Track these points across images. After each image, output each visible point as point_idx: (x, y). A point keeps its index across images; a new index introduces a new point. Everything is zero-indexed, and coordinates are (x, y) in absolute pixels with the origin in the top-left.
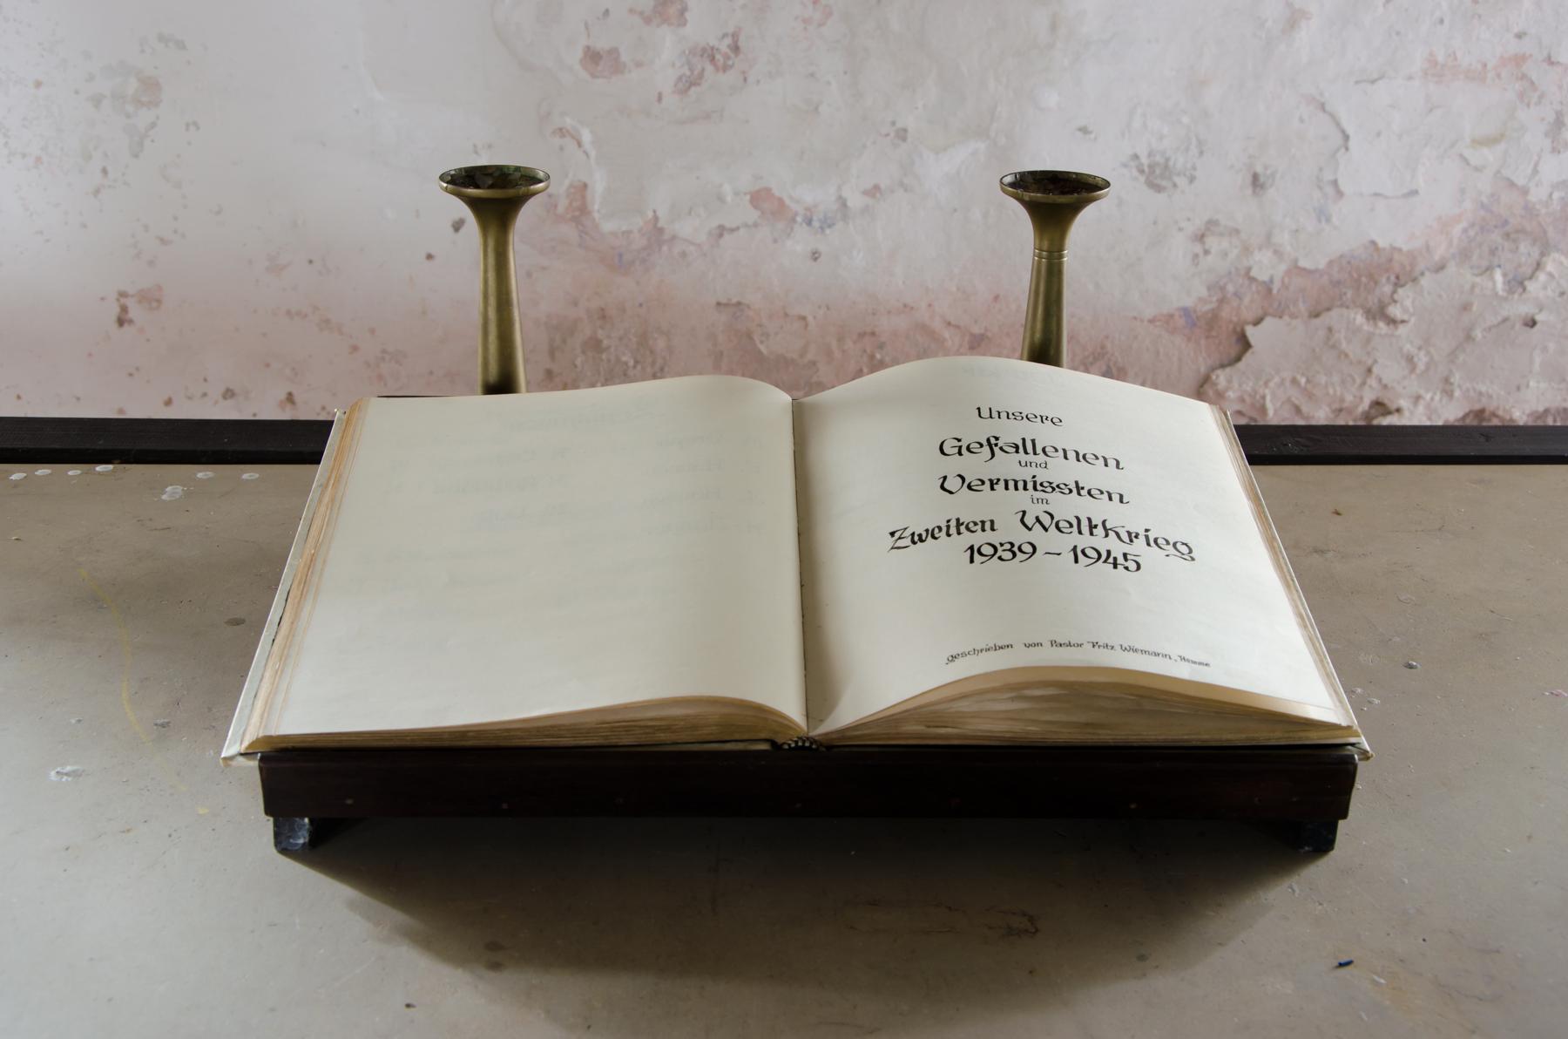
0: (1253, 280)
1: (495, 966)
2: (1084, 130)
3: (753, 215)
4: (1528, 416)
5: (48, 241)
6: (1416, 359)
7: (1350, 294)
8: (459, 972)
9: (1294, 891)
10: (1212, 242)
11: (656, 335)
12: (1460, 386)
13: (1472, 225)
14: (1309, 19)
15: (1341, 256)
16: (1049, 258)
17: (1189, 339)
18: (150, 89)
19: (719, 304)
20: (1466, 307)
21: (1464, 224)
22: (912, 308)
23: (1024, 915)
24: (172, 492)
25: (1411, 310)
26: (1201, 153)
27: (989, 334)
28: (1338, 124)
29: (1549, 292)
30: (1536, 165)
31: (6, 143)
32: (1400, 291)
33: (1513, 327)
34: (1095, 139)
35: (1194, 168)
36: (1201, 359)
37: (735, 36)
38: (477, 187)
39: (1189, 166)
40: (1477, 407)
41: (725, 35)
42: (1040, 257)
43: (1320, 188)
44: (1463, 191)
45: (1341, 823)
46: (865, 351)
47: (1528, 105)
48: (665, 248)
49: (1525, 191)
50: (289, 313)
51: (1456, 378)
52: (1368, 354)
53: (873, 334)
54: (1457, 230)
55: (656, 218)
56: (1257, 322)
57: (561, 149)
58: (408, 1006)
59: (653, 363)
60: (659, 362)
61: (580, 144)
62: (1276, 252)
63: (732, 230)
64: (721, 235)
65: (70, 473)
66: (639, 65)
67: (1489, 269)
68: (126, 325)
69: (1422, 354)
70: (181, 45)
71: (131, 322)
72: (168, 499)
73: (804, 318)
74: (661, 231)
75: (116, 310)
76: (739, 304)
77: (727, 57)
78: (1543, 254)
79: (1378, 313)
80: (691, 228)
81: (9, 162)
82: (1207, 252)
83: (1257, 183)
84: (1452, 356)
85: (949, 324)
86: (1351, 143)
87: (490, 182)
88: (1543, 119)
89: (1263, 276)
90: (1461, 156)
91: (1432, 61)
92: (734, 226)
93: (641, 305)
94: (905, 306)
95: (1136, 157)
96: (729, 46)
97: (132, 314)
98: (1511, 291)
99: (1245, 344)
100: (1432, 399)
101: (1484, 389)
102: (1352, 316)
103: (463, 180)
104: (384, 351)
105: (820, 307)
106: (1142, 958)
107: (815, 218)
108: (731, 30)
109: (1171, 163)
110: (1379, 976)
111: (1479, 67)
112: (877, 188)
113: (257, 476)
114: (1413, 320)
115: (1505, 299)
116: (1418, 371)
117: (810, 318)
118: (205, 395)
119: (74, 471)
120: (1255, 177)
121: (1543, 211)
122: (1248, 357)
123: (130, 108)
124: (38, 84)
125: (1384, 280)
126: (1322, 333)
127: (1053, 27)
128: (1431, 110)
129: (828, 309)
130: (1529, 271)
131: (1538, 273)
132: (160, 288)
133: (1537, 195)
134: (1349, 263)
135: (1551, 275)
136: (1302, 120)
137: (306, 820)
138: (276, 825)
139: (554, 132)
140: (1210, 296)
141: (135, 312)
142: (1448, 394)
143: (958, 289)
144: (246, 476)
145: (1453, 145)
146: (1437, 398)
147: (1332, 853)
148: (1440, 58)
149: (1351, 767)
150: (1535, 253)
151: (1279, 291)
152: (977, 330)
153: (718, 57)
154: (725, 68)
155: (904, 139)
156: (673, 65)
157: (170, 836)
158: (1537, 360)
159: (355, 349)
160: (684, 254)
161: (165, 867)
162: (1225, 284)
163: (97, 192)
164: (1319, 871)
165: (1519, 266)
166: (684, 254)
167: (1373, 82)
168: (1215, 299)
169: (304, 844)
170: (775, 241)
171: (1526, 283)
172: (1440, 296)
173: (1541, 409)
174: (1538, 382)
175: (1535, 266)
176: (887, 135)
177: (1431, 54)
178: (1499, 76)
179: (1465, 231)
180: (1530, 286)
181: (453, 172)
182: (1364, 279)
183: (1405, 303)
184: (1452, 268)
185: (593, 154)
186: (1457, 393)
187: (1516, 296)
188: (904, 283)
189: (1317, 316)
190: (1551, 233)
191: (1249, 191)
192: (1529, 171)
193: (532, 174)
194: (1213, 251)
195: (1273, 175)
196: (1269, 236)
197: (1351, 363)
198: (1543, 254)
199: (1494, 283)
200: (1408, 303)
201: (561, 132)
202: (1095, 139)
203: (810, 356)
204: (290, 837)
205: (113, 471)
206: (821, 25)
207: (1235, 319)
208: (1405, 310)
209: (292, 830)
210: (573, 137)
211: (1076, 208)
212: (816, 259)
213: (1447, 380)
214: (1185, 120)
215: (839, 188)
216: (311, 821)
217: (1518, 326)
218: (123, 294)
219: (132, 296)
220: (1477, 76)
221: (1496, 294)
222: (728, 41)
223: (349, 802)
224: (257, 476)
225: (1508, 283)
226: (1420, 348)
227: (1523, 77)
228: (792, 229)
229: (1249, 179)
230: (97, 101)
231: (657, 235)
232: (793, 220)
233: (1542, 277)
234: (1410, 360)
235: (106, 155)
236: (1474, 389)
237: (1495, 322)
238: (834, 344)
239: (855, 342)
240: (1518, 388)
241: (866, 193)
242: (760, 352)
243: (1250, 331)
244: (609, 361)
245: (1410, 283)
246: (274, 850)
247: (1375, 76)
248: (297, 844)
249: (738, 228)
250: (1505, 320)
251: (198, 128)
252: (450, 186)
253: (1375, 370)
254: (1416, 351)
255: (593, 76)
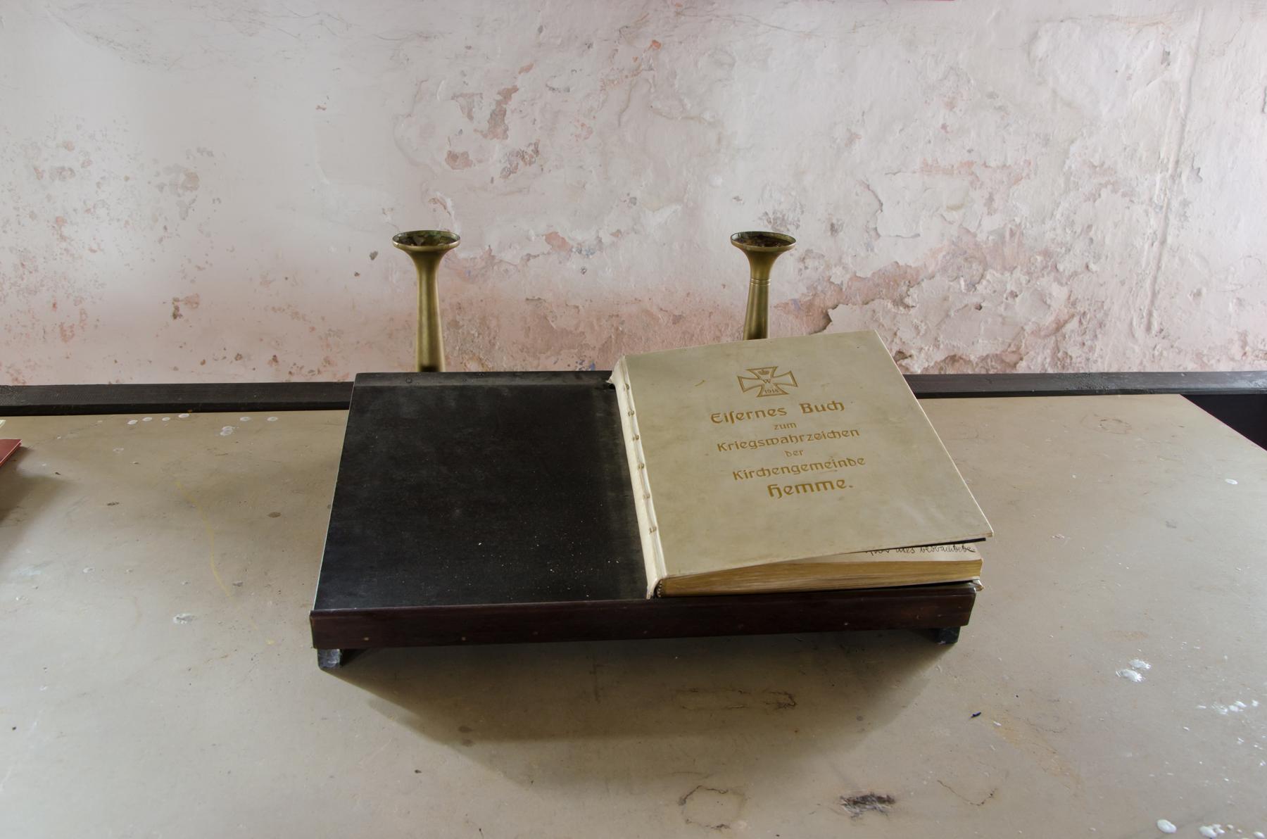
0: (832, 283)
1: (467, 743)
2: (737, 199)
3: (547, 248)
4: (978, 358)
5: (132, 269)
6: (920, 328)
7: (884, 291)
8: (446, 747)
9: (939, 670)
10: (809, 262)
11: (491, 318)
12: (943, 343)
13: (948, 253)
14: (860, 138)
15: (880, 270)
16: (760, 284)
17: (797, 317)
18: (192, 180)
19: (527, 299)
20: (946, 299)
21: (944, 253)
22: (640, 301)
23: (786, 694)
24: (226, 430)
25: (917, 300)
26: (803, 212)
27: (684, 315)
28: (877, 197)
29: (988, 291)
30: (980, 222)
31: (108, 213)
32: (911, 289)
33: (970, 309)
34: (744, 203)
35: (799, 221)
36: (803, 329)
37: (536, 145)
38: (415, 244)
39: (796, 219)
40: (952, 354)
41: (530, 144)
42: (755, 283)
43: (867, 232)
44: (943, 235)
45: (963, 628)
46: (613, 326)
47: (975, 189)
48: (495, 267)
49: (975, 236)
50: (273, 308)
51: (941, 338)
52: (895, 324)
53: (618, 316)
54: (940, 257)
55: (490, 250)
56: (835, 307)
57: (434, 210)
58: (417, 772)
59: (490, 334)
60: (493, 334)
61: (445, 208)
62: (844, 268)
63: (535, 257)
64: (528, 260)
65: (164, 419)
66: (480, 161)
67: (957, 278)
68: (178, 318)
69: (923, 324)
70: (210, 154)
71: (181, 316)
72: (224, 435)
73: (577, 307)
74: (493, 257)
75: (172, 309)
76: (539, 299)
77: (531, 157)
78: (984, 270)
79: (900, 302)
80: (511, 256)
81: (110, 224)
82: (806, 268)
83: (833, 229)
84: (939, 326)
85: (661, 309)
86: (884, 207)
87: (422, 240)
88: (983, 197)
89: (837, 282)
90: (942, 215)
91: (925, 163)
92: (536, 254)
93: (482, 301)
94: (636, 299)
95: (766, 214)
96: (532, 150)
97: (181, 311)
98: (969, 290)
99: (828, 320)
100: (929, 349)
101: (955, 344)
102: (885, 304)
103: (408, 240)
104: (330, 330)
105: (586, 300)
106: (860, 719)
107: (583, 249)
108: (533, 141)
109: (786, 218)
110: (997, 721)
111: (950, 167)
112: (619, 231)
113: (276, 419)
114: (918, 306)
115: (966, 294)
116: (921, 334)
117: (581, 307)
118: (225, 358)
119: (166, 418)
120: (832, 225)
121: (984, 246)
122: (829, 327)
123: (180, 191)
124: (127, 179)
125: (902, 283)
126: (870, 313)
127: (719, 141)
128: (925, 190)
129: (591, 301)
130: (978, 279)
131: (982, 280)
132: (198, 296)
133: (981, 237)
134: (884, 274)
135: (988, 281)
136: (857, 194)
137: (338, 650)
138: (319, 653)
139: (430, 201)
140: (808, 293)
141: (183, 310)
142: (937, 347)
143: (666, 290)
144: (270, 419)
145: (937, 210)
146: (931, 349)
147: (957, 644)
148: (930, 162)
149: (972, 595)
150: (981, 271)
151: (846, 289)
152: (677, 313)
153: (526, 157)
154: (531, 163)
155: (635, 204)
156: (500, 161)
157: (252, 659)
158: (983, 328)
159: (313, 329)
160: (506, 271)
161: (252, 681)
162: (817, 286)
163: (161, 240)
164: (952, 654)
165: (973, 276)
166: (506, 271)
167: (895, 174)
168: (811, 294)
169: (337, 664)
170: (560, 263)
171: (976, 285)
172: (932, 293)
173: (985, 355)
174: (983, 340)
175: (980, 276)
176: (625, 201)
177: (925, 160)
178: (960, 172)
179: (944, 257)
180: (978, 287)
181: (400, 235)
182: (892, 283)
183: (914, 297)
184: (938, 277)
185: (453, 213)
186: (942, 346)
187: (971, 292)
188: (635, 286)
189: (867, 303)
190: (988, 258)
191: (829, 233)
192: (977, 224)
193: (448, 236)
194: (810, 267)
195: (842, 225)
196: (840, 259)
197: (885, 330)
198: (984, 270)
199: (960, 285)
200: (915, 296)
201: (435, 201)
202: (744, 203)
203: (581, 329)
204: (328, 660)
205: (189, 417)
206: (586, 138)
207: (822, 306)
208: (914, 301)
209: (329, 655)
210: (441, 204)
211: (775, 255)
212: (584, 273)
213: (936, 339)
214: (794, 193)
215: (598, 232)
216: (341, 650)
217: (973, 309)
218: (176, 300)
219: (182, 301)
220: (949, 172)
221: (961, 291)
222: (532, 147)
223: (367, 639)
224: (276, 419)
225: (967, 285)
226: (922, 322)
227: (972, 173)
228: (570, 256)
229: (829, 227)
230: (161, 188)
231: (491, 259)
232: (571, 251)
233: (984, 282)
234: (917, 328)
235: (166, 219)
236: (950, 344)
237: (961, 307)
238: (595, 321)
239: (607, 321)
240: (973, 343)
241: (613, 234)
242: (552, 327)
243: (831, 312)
244: (463, 333)
245: (916, 286)
246: (318, 668)
247: (896, 171)
248: (332, 664)
249: (538, 256)
250: (966, 306)
251: (220, 202)
252: (400, 244)
253: (898, 333)
254: (920, 323)
255: (453, 168)
